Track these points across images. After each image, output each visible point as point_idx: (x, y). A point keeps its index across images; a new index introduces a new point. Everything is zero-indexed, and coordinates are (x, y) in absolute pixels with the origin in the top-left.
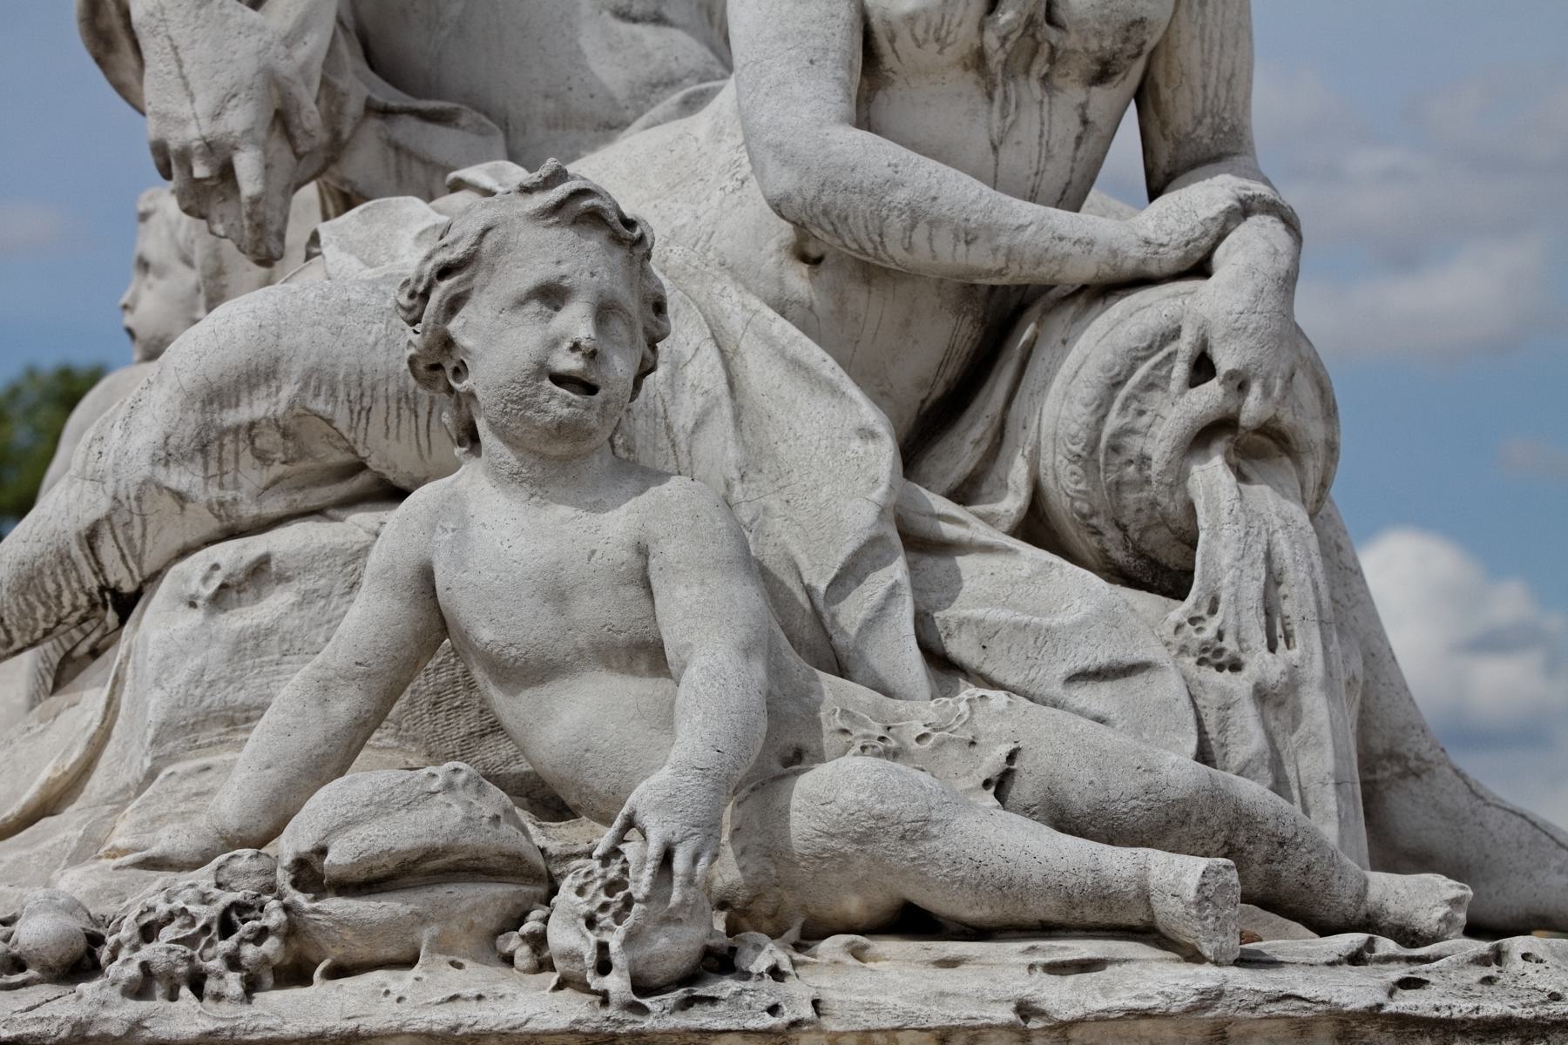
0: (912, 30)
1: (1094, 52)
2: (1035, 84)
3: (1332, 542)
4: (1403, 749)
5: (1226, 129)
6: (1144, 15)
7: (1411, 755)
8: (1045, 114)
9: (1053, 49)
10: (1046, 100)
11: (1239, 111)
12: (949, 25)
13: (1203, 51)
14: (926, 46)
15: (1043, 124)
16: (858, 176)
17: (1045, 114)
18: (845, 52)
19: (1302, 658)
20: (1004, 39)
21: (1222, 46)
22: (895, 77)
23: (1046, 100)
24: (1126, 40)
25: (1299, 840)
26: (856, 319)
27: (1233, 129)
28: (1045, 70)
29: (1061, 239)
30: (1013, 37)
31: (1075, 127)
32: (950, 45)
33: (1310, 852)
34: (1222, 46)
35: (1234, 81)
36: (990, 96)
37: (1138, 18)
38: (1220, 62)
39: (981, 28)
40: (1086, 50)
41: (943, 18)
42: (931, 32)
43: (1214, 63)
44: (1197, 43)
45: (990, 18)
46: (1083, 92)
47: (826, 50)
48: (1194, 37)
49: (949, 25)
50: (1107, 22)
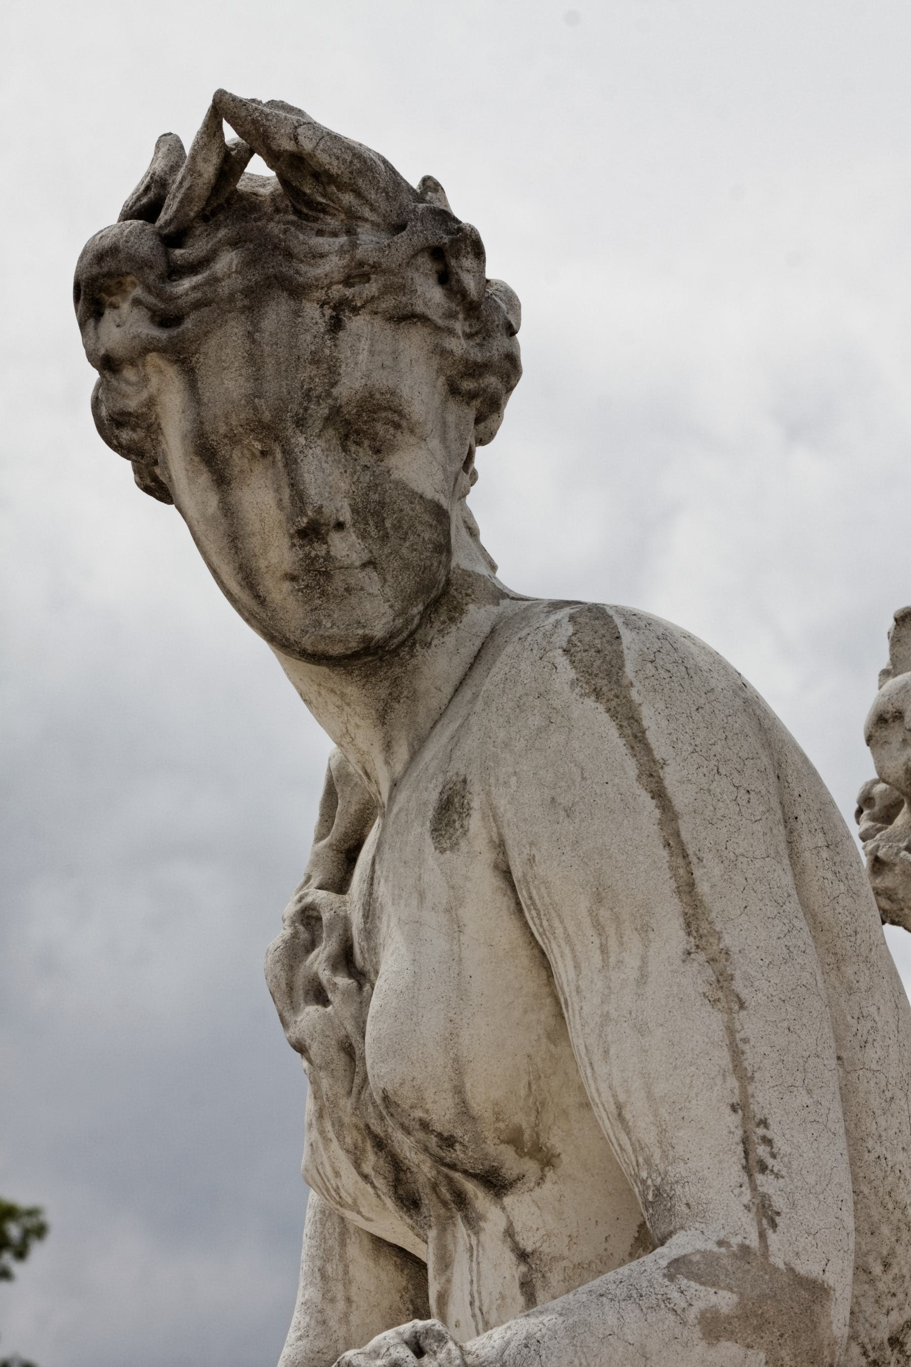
11: (657, 1158)
31: (512, 1270)
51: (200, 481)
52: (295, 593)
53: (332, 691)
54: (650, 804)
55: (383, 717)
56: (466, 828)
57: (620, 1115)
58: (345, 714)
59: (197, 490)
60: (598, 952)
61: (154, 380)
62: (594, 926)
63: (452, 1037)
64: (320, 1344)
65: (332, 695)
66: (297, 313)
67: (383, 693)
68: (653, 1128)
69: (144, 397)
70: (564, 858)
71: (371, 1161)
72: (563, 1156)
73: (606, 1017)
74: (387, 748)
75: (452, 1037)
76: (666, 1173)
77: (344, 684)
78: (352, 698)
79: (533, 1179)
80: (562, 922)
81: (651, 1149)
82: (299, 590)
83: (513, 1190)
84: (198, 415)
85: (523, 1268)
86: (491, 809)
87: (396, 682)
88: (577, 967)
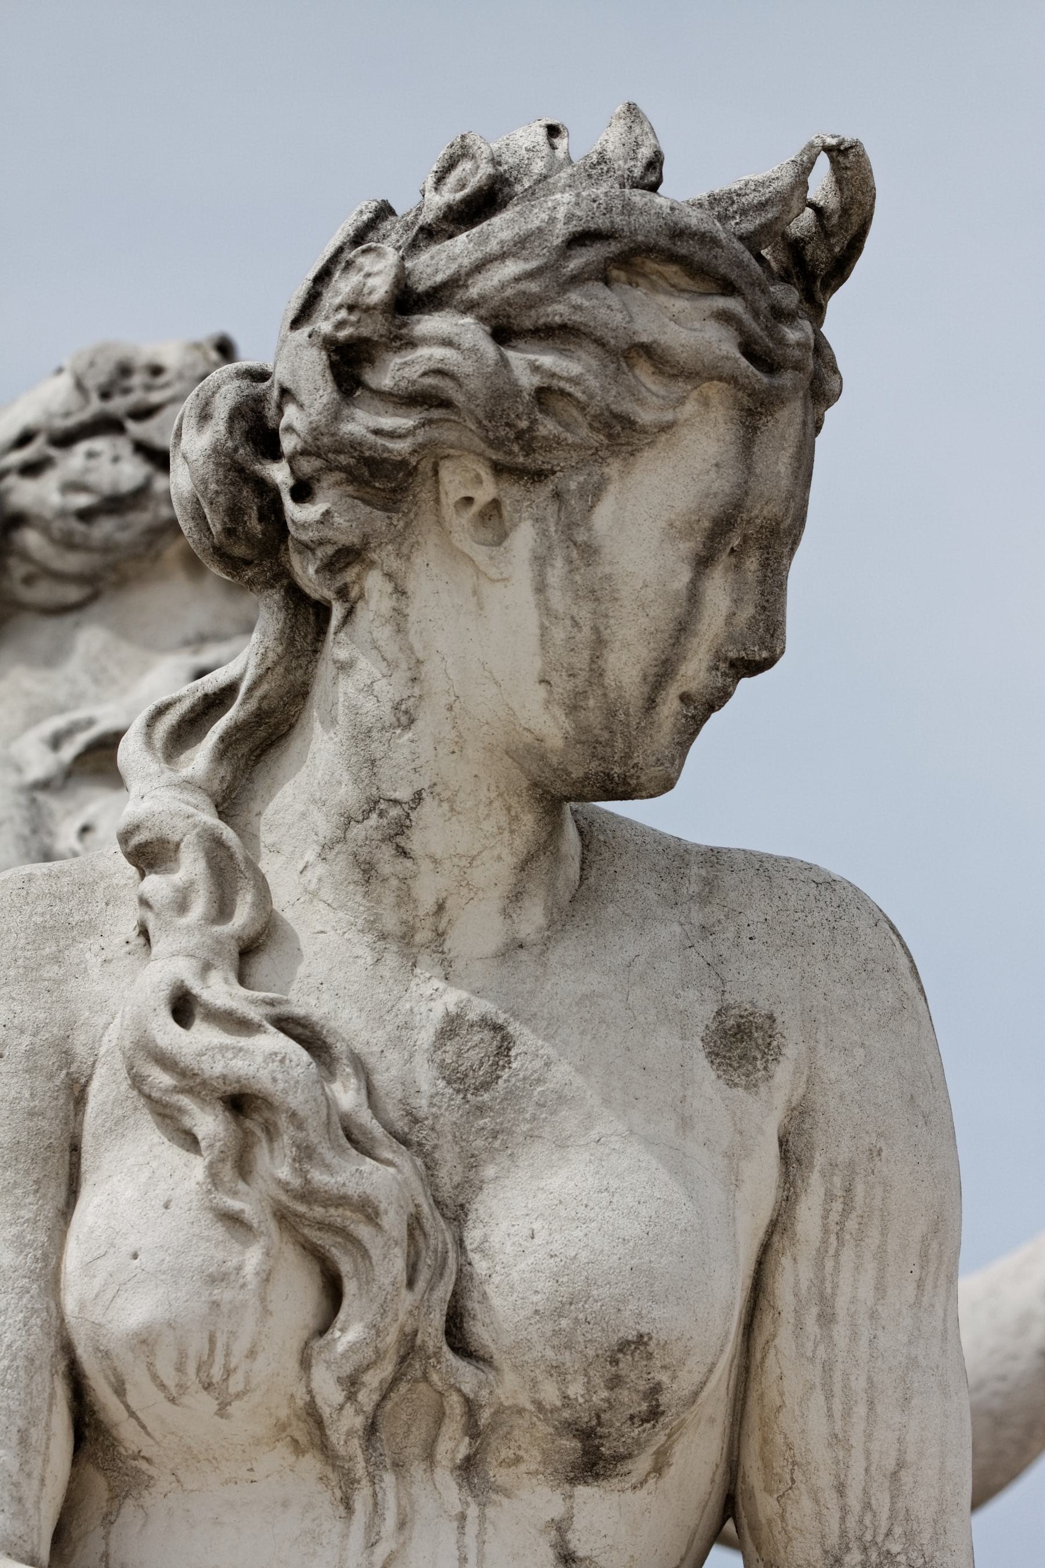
0: (150, 1365)
1: (554, 1410)
2: (446, 1480)
6: (644, 1329)
8: (470, 1540)
9: (471, 1407)
10: (473, 1511)
11: (925, 1537)
12: (227, 1355)
13: (830, 1416)
14: (185, 1400)
17: (470, 1540)
20: (352, 1383)
21: (871, 1404)
22: (152, 1471)
23: (473, 1511)
24: (615, 1382)
28: (463, 1451)
30: (373, 1380)
32: (238, 1396)
34: (871, 1404)
35: (906, 1476)
36: (347, 1503)
37: (632, 1336)
38: (869, 1436)
39: (305, 1363)
40: (539, 1406)
41: (212, 1341)
42: (191, 1368)
43: (857, 1440)
44: (818, 1399)
45: (322, 1342)
46: (557, 1498)
48: (813, 1387)
49: (227, 1355)
50: (568, 1346)
51: (681, 546)
52: (680, 717)
53: (509, 809)
56: (770, 1074)
57: (894, 1476)
58: (498, 838)
59: (671, 553)
60: (915, 1285)
61: (690, 408)
62: (920, 1256)
65: (505, 812)
68: (934, 1503)
69: (667, 418)
70: (917, 1168)
72: (672, 1468)
73: (913, 1362)
74: (514, 899)
76: (933, 1558)
77: (527, 809)
78: (523, 828)
79: (634, 1481)
80: (884, 1233)
81: (922, 1526)
82: (686, 716)
83: (604, 1483)
84: (746, 482)
86: (810, 1068)
88: (880, 1289)
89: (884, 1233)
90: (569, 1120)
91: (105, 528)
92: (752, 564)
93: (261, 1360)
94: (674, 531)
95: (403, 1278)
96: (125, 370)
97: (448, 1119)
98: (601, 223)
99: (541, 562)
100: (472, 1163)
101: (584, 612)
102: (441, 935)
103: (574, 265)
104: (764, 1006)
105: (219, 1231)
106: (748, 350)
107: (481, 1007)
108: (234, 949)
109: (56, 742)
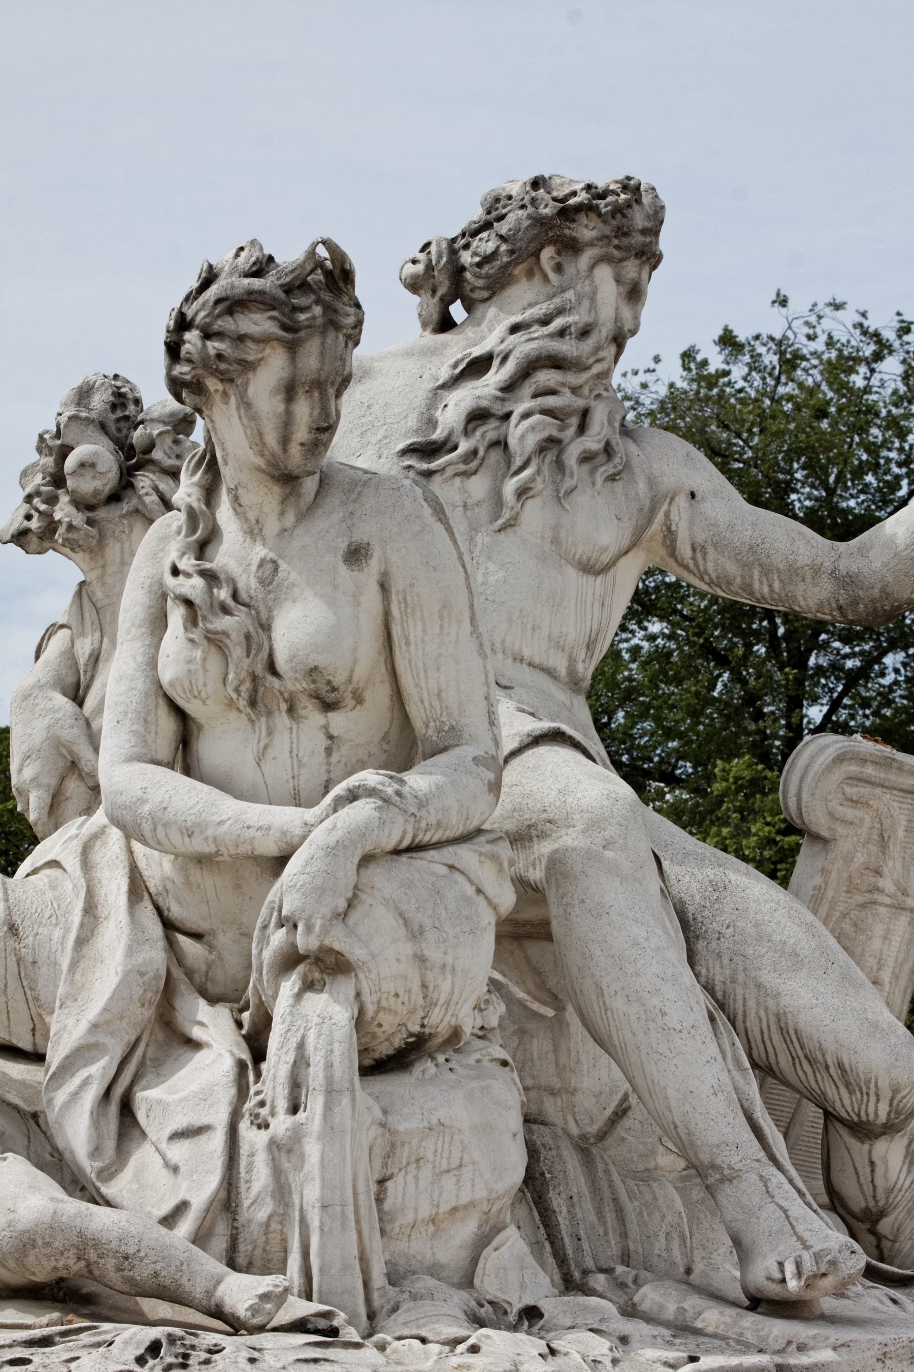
2: (285, 716)
3: (657, 1010)
4: (719, 1161)
5: (446, 729)
7: (725, 1166)
8: (294, 736)
11: (456, 713)
15: (292, 743)
16: (123, 798)
17: (294, 736)
18: (139, 712)
19: (307, 1118)
20: (237, 690)
21: (426, 672)
23: (295, 726)
25: (142, 1254)
26: (199, 887)
27: (452, 728)
29: (249, 827)
33: (155, 1263)
34: (426, 672)
35: (443, 695)
38: (427, 683)
43: (423, 684)
44: (409, 671)
47: (126, 713)
54: (462, 570)
55: (283, 501)
57: (439, 695)
63: (355, 650)
64: (144, 750)
66: (337, 337)
67: (288, 491)
71: (248, 685)
75: (355, 650)
80: (422, 611)
85: (329, 742)
87: (293, 487)
88: (424, 631)
89: (422, 611)
90: (296, 591)
91: (486, 269)
92: (316, 394)
93: (209, 687)
94: (274, 392)
95: (244, 654)
96: (497, 200)
97: (261, 596)
98: (224, 295)
99: (238, 408)
100: (270, 610)
101: (253, 424)
102: (261, 530)
103: (217, 311)
104: (366, 540)
105: (189, 645)
106: (285, 328)
107: (272, 555)
108: (197, 546)
109: (455, 365)
